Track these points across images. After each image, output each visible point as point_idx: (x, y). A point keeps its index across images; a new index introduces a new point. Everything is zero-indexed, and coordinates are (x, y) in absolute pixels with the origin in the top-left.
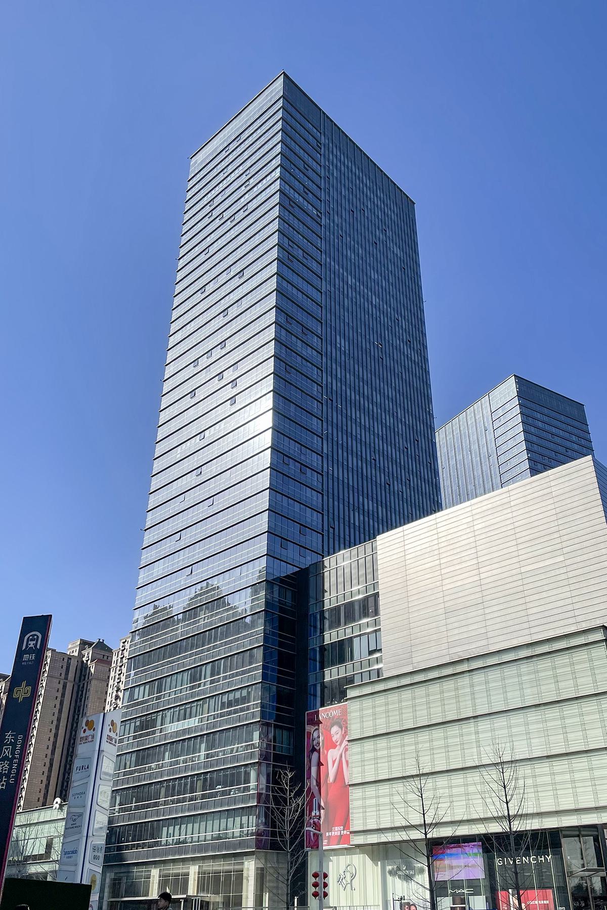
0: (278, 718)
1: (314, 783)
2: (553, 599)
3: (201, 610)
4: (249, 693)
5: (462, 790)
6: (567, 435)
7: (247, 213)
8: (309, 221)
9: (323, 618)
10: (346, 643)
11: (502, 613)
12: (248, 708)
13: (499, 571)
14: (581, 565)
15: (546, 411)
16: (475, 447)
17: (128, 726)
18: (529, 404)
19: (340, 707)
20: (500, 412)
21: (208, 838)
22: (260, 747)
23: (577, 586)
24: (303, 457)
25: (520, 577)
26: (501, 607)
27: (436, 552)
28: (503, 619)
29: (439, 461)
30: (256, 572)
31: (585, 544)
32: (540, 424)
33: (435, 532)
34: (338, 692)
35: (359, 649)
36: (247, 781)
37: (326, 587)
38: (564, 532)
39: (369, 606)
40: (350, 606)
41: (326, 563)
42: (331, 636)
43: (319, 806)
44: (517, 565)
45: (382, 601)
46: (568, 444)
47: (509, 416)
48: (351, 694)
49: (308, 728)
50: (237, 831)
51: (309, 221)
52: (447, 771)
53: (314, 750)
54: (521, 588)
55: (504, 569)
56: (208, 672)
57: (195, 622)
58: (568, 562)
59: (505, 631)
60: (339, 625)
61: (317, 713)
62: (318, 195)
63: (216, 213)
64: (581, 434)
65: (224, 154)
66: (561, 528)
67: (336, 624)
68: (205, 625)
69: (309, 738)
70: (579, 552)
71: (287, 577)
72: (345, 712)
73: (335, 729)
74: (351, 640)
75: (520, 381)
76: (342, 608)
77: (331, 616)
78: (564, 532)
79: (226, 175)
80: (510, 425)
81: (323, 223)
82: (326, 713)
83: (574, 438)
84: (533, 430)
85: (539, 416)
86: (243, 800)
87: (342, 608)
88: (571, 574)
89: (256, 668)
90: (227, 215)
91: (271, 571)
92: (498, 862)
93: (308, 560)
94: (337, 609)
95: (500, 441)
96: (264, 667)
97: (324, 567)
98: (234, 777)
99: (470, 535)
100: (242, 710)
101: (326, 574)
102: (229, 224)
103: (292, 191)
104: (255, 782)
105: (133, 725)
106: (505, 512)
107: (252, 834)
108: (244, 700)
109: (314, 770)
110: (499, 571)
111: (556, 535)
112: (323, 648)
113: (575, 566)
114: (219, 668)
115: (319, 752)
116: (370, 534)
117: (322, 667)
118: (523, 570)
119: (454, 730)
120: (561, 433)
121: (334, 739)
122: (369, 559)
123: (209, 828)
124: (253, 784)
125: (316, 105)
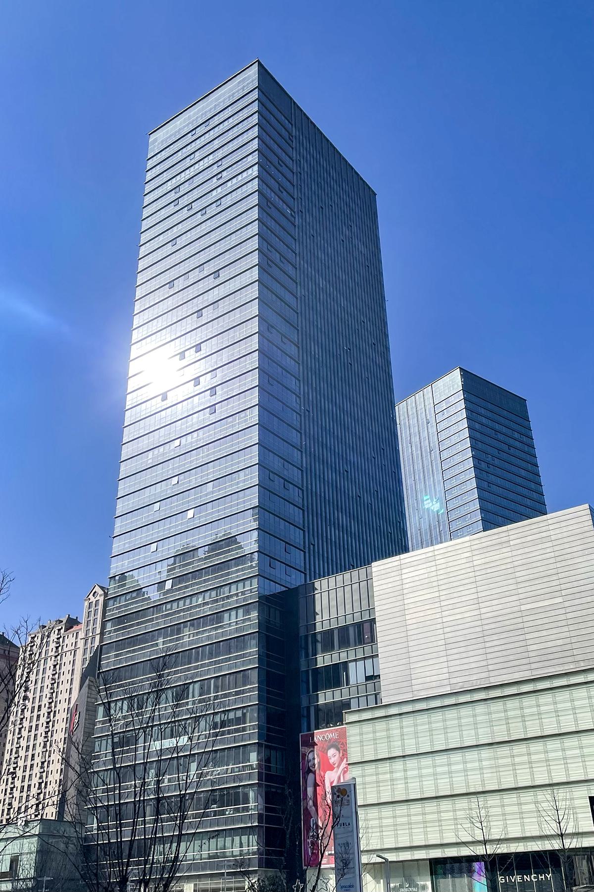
0: (269, 739)
1: (311, 803)
2: (553, 637)
3: (185, 627)
4: (244, 715)
5: (405, 820)
6: (509, 432)
7: (220, 209)
8: (284, 222)
9: (315, 641)
10: (341, 666)
11: (503, 647)
12: (244, 729)
13: (500, 607)
14: (580, 607)
15: (490, 406)
16: (416, 439)
17: (104, 742)
18: (474, 399)
19: (337, 730)
20: (444, 405)
21: (203, 856)
22: (259, 766)
23: (576, 627)
24: (286, 472)
25: (519, 614)
26: (502, 642)
27: (435, 584)
28: (504, 653)
29: (403, 471)
30: (251, 590)
31: (582, 588)
32: (484, 420)
33: (433, 563)
34: (334, 715)
35: (356, 673)
36: (246, 801)
37: (318, 609)
38: (563, 575)
39: (362, 633)
40: (344, 630)
41: (317, 585)
42: (323, 660)
43: (317, 826)
44: (518, 603)
45: (379, 627)
46: (512, 441)
47: (453, 410)
48: (349, 718)
49: (302, 749)
50: (236, 850)
51: (284, 222)
52: (436, 798)
53: (309, 771)
54: (521, 626)
55: (505, 606)
56: (197, 692)
57: (178, 639)
58: (567, 604)
59: (506, 665)
60: (333, 648)
61: (312, 735)
62: (291, 191)
63: (184, 201)
64: (523, 430)
65: (189, 138)
66: (560, 570)
67: (328, 646)
68: (190, 643)
69: (304, 758)
70: (578, 596)
71: (273, 595)
72: (343, 735)
73: (331, 752)
74: (346, 664)
75: (465, 374)
76: (336, 632)
77: (323, 639)
78: (563, 575)
79: (193, 162)
80: (454, 420)
81: (297, 223)
82: (321, 735)
83: (516, 435)
84: (477, 426)
85: (483, 411)
86: (242, 820)
87: (336, 632)
88: (569, 616)
89: (250, 690)
90: (196, 206)
91: (262, 591)
92: (501, 880)
93: (296, 580)
94: (330, 632)
95: (442, 436)
96: (260, 689)
97: (314, 589)
98: (230, 797)
99: (469, 570)
100: (237, 731)
101: (317, 597)
102: (199, 218)
103: (269, 191)
104: (254, 803)
105: (110, 741)
106: (504, 550)
107: (254, 853)
108: (238, 721)
109: (310, 790)
110: (500, 607)
111: (555, 577)
112: (317, 671)
113: (574, 608)
114: (209, 688)
115: (314, 773)
116: (366, 561)
117: (316, 689)
118: (523, 608)
119: (456, 757)
120: (504, 430)
121: (331, 761)
122: (363, 584)
123: (205, 847)
124: (252, 805)
125: (273, 79)
